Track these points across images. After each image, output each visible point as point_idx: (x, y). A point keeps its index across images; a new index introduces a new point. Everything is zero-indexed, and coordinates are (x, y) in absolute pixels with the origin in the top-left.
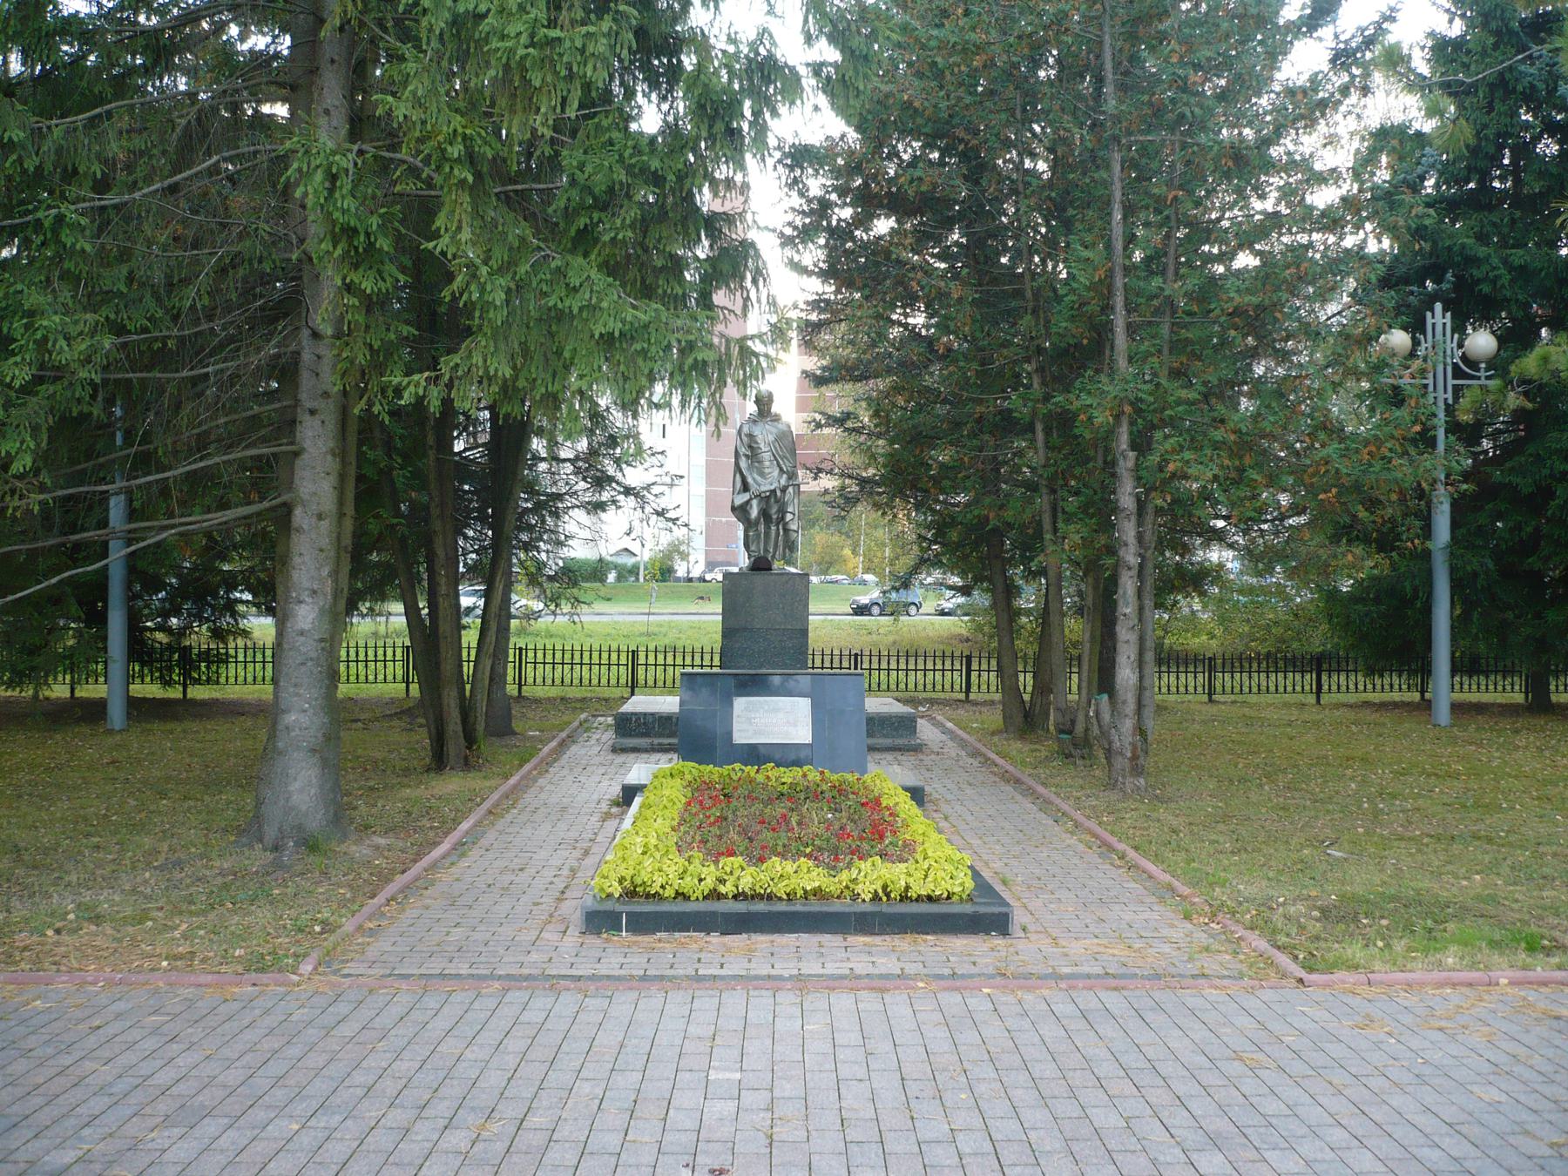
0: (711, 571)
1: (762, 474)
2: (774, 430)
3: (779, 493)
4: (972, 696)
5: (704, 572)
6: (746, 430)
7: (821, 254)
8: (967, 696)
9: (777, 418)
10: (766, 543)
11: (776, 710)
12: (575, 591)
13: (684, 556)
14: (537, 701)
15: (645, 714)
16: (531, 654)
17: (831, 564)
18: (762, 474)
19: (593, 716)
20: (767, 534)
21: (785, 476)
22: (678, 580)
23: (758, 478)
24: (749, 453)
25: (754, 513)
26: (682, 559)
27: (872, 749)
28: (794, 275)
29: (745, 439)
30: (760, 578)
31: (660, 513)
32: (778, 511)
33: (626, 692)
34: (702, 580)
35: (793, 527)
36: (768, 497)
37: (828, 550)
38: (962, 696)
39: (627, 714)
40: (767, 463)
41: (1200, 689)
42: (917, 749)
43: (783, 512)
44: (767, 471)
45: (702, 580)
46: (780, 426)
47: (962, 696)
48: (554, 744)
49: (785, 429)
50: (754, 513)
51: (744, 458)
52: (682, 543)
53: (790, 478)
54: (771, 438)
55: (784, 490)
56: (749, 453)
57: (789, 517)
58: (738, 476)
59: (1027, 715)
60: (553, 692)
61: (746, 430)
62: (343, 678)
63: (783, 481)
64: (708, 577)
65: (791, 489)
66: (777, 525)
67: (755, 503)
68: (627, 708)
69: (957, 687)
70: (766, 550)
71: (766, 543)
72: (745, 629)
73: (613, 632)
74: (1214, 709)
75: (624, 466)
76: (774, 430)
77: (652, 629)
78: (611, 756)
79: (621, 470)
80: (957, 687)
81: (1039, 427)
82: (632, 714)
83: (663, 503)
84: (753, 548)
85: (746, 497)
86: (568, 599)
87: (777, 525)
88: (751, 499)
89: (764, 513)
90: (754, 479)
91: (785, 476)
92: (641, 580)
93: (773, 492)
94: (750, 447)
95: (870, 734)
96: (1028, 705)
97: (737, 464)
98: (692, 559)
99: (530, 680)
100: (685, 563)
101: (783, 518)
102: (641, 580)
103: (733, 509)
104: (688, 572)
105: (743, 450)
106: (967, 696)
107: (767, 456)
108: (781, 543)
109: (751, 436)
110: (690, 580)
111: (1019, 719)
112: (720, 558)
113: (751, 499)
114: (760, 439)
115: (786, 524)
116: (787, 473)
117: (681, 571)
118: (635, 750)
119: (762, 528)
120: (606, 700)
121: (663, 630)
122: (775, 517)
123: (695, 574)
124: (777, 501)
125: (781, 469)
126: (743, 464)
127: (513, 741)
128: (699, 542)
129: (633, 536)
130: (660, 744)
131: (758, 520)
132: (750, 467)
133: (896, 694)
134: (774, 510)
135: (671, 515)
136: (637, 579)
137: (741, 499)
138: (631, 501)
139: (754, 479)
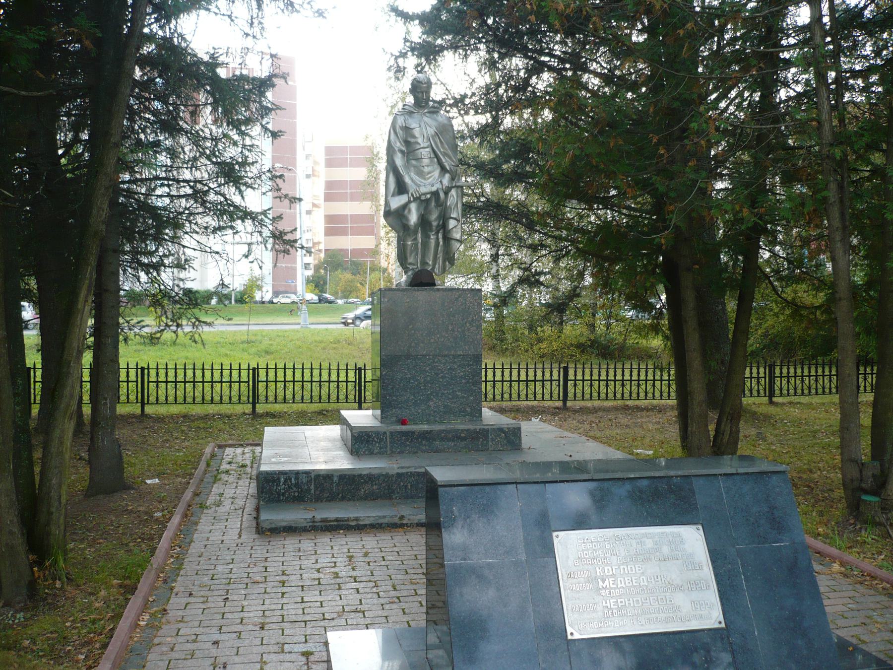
0: (277, 296)
1: (421, 174)
2: (433, 123)
3: (442, 195)
4: (569, 404)
5: (272, 297)
6: (400, 121)
8: (565, 404)
10: (424, 256)
12: (196, 311)
13: (260, 288)
14: (160, 419)
16: (153, 373)
17: (350, 292)
19: (220, 447)
20: (425, 245)
21: (447, 176)
22: (256, 302)
26: (259, 290)
28: (11, 520)
30: (422, 295)
32: (439, 218)
34: (271, 302)
36: (427, 201)
37: (349, 283)
38: (559, 404)
40: (426, 161)
41: (762, 392)
44: (426, 169)
45: (271, 302)
47: (559, 404)
48: (176, 520)
49: (446, 122)
51: (399, 155)
52: (258, 280)
53: (453, 179)
54: (431, 131)
57: (452, 223)
60: (175, 409)
62: (571, 395)
64: (275, 301)
65: (453, 192)
66: (437, 233)
67: (413, 206)
69: (555, 396)
70: (424, 263)
71: (424, 256)
72: (408, 356)
73: (222, 340)
74: (772, 410)
75: (243, 188)
77: (252, 338)
79: (241, 192)
80: (555, 396)
85: (403, 199)
86: (189, 319)
89: (424, 221)
91: (447, 176)
92: (233, 302)
93: (435, 194)
98: (264, 289)
99: (152, 399)
100: (260, 292)
102: (233, 302)
103: (388, 214)
104: (262, 298)
105: (398, 145)
106: (565, 404)
109: (407, 129)
110: (263, 303)
112: (281, 289)
113: (409, 202)
114: (417, 132)
117: (258, 296)
118: (291, 530)
120: (229, 417)
121: (259, 338)
122: (435, 224)
123: (267, 298)
126: (399, 161)
127: (124, 500)
128: (269, 279)
129: (251, 258)
130: (324, 520)
132: (407, 166)
133: (494, 404)
134: (434, 216)
136: (231, 303)
137: (397, 202)
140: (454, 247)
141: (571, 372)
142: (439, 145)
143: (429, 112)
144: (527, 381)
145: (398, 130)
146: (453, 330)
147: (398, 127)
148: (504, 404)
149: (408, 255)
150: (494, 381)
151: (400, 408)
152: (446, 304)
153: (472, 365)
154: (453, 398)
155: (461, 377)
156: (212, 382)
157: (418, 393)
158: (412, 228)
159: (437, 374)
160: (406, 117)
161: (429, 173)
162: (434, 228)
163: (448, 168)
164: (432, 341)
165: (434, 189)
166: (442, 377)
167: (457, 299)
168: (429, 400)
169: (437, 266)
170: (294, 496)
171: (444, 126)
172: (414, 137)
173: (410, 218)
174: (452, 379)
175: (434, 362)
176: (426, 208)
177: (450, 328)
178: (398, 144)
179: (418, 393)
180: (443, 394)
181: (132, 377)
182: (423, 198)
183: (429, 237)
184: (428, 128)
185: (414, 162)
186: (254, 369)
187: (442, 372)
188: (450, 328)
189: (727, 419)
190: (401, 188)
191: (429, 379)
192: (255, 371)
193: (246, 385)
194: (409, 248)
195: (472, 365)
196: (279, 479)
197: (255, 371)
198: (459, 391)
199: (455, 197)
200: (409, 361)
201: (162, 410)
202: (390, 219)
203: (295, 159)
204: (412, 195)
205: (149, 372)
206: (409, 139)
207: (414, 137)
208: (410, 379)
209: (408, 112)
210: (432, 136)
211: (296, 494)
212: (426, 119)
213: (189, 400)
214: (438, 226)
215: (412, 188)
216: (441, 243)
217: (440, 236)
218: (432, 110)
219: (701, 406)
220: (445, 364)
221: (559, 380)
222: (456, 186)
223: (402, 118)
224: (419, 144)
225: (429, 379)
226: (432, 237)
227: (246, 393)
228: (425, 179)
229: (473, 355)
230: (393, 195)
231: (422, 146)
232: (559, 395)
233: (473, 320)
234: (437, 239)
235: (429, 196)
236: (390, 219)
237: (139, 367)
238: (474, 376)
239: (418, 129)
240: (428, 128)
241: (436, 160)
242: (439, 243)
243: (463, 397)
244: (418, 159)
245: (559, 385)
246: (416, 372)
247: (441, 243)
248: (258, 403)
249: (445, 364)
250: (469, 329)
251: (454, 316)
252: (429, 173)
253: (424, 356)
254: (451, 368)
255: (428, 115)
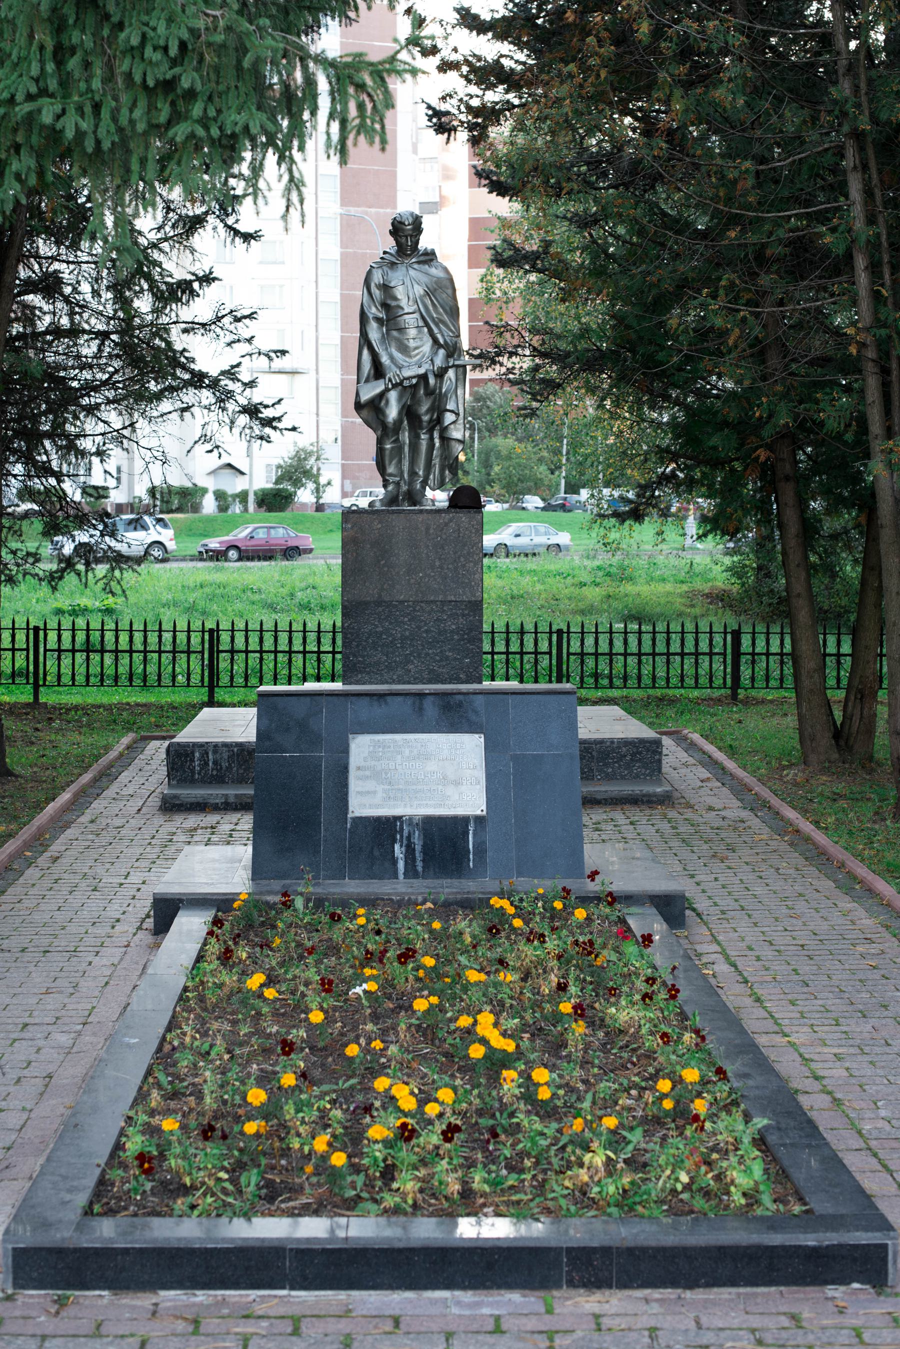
2: (424, 279)
3: (432, 381)
4: (741, 693)
6: (377, 277)
7: (489, 580)
9: (430, 257)
11: (427, 757)
15: (216, 746)
16: (52, 636)
18: (404, 349)
21: (442, 352)
23: (398, 355)
24: (382, 315)
25: (392, 412)
27: (590, 802)
29: (376, 293)
31: (252, 411)
32: (431, 410)
33: (199, 695)
35: (457, 433)
36: (415, 387)
39: (187, 745)
40: (412, 332)
42: (666, 800)
43: (439, 409)
44: (412, 344)
46: (433, 271)
50: (392, 412)
52: (310, 454)
53: (449, 355)
54: (419, 290)
55: (440, 374)
56: (382, 315)
57: (449, 418)
58: (366, 352)
59: (838, 735)
61: (377, 277)
62: (225, 679)
63: (439, 361)
65: (451, 373)
66: (430, 432)
67: (393, 396)
68: (189, 734)
69: (718, 682)
70: (413, 473)
72: (379, 603)
76: (424, 279)
78: (159, 820)
80: (718, 682)
81: (860, 262)
82: (195, 745)
83: (257, 396)
84: (391, 469)
85: (378, 387)
87: (430, 432)
88: (387, 390)
89: (409, 412)
90: (392, 358)
93: (424, 378)
94: (385, 306)
95: (587, 776)
96: (838, 715)
97: (364, 334)
101: (439, 420)
105: (373, 311)
107: (411, 321)
108: (436, 461)
109: (386, 288)
111: (825, 740)
113: (387, 390)
114: (400, 292)
115: (444, 430)
116: (445, 346)
118: (200, 807)
119: (405, 437)
122: (426, 418)
124: (429, 393)
125: (435, 341)
126: (374, 334)
131: (398, 423)
135: (267, 413)
136: (246, 510)
137: (369, 392)
138: (207, 396)
139: (392, 358)
140: (454, 450)
141: (746, 641)
142: (431, 308)
143: (418, 263)
144: (697, 654)
145: (374, 289)
146: (441, 567)
147: (373, 285)
148: (637, 694)
149: (387, 462)
150: (145, 652)
151: (368, 673)
152: (431, 531)
153: (468, 615)
154: (441, 660)
155: (452, 632)
156: (261, 652)
157: (393, 653)
158: (390, 426)
159: (419, 628)
160: (385, 268)
161: (416, 348)
162: (425, 424)
163: (442, 341)
164: (412, 581)
165: (422, 371)
166: (427, 631)
167: (446, 524)
168: (409, 662)
169: (431, 477)
170: (212, 775)
171: (438, 281)
172: (396, 299)
173: (388, 412)
174: (440, 633)
175: (415, 610)
176: (414, 396)
177: (437, 564)
178: (374, 310)
179: (393, 653)
180: (427, 654)
181: (544, 646)
182: (406, 383)
183: (418, 437)
184: (416, 286)
185: (395, 333)
186: (211, 631)
187: (426, 624)
188: (437, 564)
189: (856, 698)
190: (378, 371)
191: (407, 633)
192: (214, 634)
193: (199, 657)
194: (387, 453)
195: (468, 615)
196: (193, 753)
197: (214, 634)
198: (450, 650)
199: (454, 380)
200: (380, 609)
201: (73, 698)
202: (365, 412)
203: (394, 175)
204: (390, 380)
205: (46, 635)
206: (389, 302)
207: (395, 299)
208: (381, 633)
209: (389, 263)
210: (421, 298)
211: (215, 773)
212: (412, 272)
213: (80, 679)
214: (431, 420)
215: (392, 373)
216: (437, 444)
217: (436, 435)
218: (422, 258)
219: (812, 677)
220: (430, 613)
221: (724, 654)
222: (453, 366)
223: (380, 271)
224: (402, 309)
225: (407, 633)
226: (423, 437)
227: (49, 664)
228: (410, 357)
229: (470, 602)
230: (367, 381)
231: (406, 311)
232: (725, 679)
233: (469, 553)
234: (431, 439)
235: (414, 381)
236: (365, 412)
237: (554, 628)
238: (471, 630)
239: (400, 288)
240: (416, 286)
241: (426, 330)
242: (434, 445)
243: (456, 659)
244: (401, 330)
245: (725, 662)
246: (391, 623)
247: (437, 444)
248: (218, 686)
249: (430, 613)
250: (464, 566)
251: (442, 548)
252: (416, 348)
253: (402, 602)
254: (438, 620)
255: (416, 266)
